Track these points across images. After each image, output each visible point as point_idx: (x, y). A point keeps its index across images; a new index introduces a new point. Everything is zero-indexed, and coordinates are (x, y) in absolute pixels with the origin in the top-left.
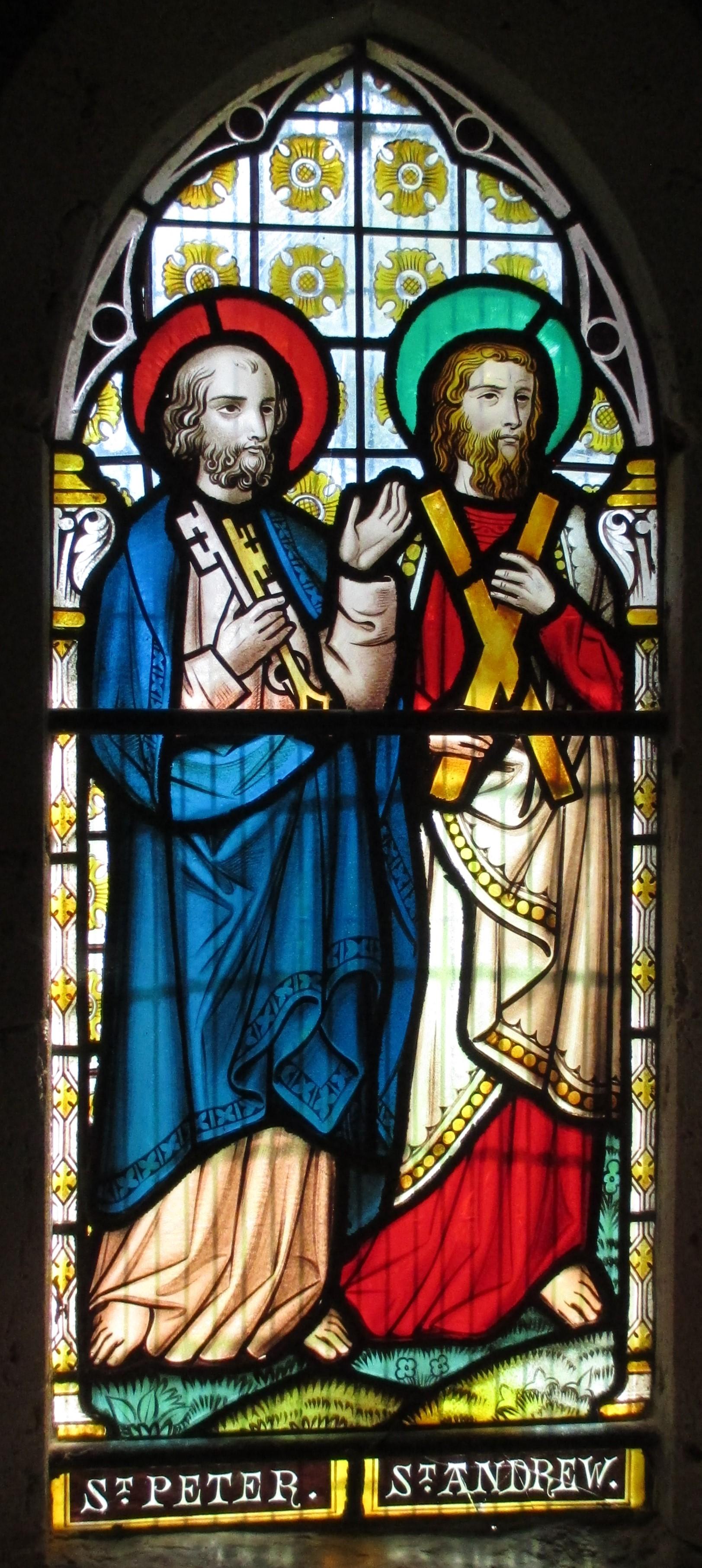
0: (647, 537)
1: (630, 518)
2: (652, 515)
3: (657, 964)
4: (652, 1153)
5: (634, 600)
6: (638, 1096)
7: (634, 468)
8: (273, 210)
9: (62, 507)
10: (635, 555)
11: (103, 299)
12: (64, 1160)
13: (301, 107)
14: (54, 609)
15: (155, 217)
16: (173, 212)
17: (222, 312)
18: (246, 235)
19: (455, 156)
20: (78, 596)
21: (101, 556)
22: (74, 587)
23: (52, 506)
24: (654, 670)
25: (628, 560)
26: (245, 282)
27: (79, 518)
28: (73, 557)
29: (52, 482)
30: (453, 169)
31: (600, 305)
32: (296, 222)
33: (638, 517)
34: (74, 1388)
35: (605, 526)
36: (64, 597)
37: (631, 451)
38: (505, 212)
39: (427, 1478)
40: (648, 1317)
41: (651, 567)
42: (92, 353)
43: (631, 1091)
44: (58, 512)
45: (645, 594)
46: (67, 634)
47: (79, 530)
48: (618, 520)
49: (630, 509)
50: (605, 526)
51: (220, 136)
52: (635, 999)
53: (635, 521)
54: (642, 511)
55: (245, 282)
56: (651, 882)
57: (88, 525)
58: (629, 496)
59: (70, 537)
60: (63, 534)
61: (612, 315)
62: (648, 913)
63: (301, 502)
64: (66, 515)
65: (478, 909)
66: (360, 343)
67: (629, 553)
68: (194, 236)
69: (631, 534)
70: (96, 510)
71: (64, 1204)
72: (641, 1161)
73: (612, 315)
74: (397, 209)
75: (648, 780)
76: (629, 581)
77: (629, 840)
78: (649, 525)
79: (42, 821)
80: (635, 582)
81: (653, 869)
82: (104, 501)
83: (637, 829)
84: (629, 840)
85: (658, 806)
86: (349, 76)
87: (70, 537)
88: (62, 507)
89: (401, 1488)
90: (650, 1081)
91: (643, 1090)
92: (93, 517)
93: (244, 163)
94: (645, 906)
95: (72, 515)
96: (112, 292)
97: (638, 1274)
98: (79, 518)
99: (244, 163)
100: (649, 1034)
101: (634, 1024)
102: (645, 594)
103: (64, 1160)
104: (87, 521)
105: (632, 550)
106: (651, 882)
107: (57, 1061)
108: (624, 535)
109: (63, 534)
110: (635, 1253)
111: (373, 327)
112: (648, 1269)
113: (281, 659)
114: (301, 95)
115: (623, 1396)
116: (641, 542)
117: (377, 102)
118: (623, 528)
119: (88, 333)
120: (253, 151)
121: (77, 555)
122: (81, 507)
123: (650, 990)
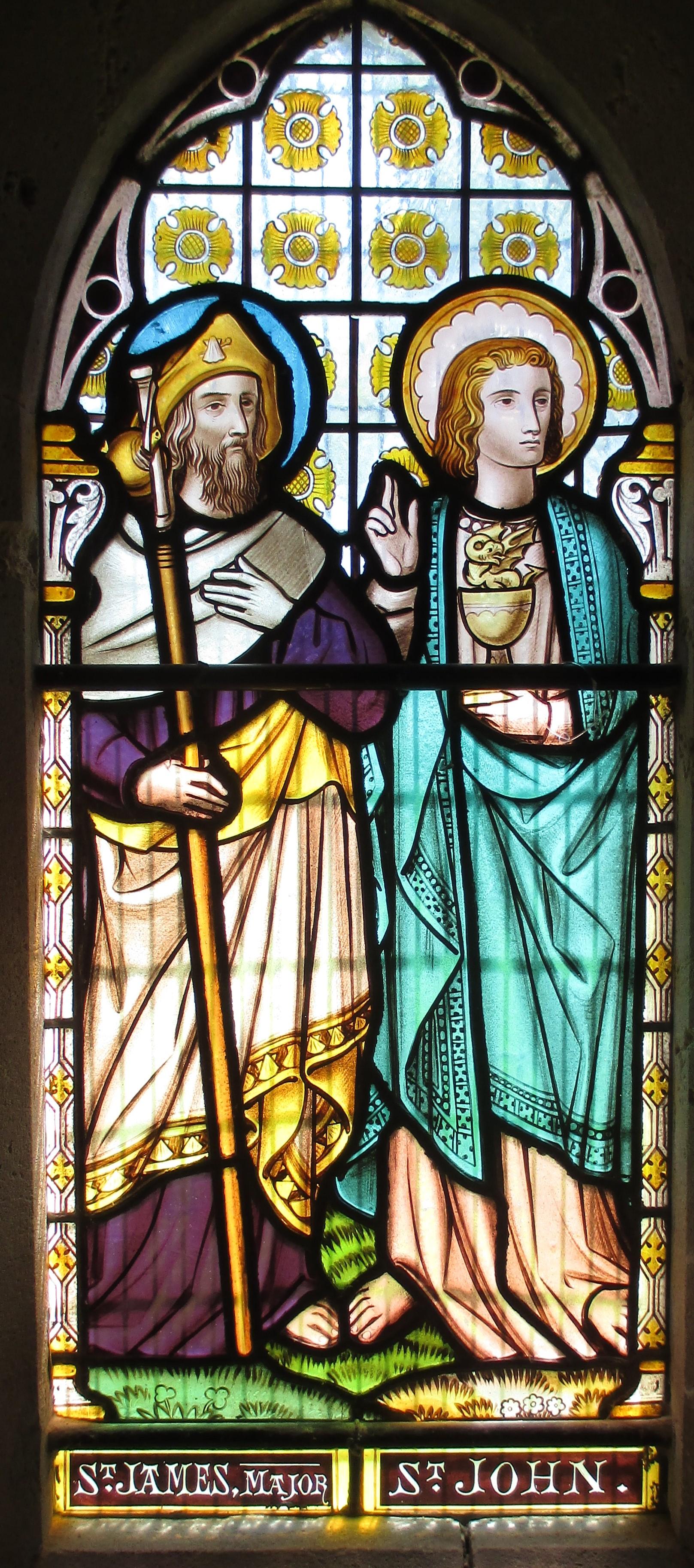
0: (663, 506)
3: (668, 1160)
4: (665, 1152)
5: (649, 575)
7: (651, 433)
9: (52, 478)
10: (649, 525)
11: (93, 272)
12: (55, 762)
15: (151, 184)
16: (171, 176)
20: (70, 573)
21: (92, 527)
22: (66, 563)
23: (41, 476)
25: (644, 532)
27: (70, 489)
28: (67, 528)
29: (40, 453)
30: (456, 125)
33: (654, 485)
34: (71, 1370)
36: (55, 572)
38: (516, 166)
39: (436, 1476)
40: (662, 1060)
41: (666, 558)
42: (83, 324)
44: (48, 484)
45: (659, 570)
46: (57, 608)
47: (72, 504)
48: (634, 487)
50: (619, 487)
52: (648, 989)
53: (651, 491)
56: (668, 781)
57: (80, 498)
58: (644, 465)
59: (61, 512)
60: (54, 507)
63: (306, 478)
64: (60, 487)
68: (191, 218)
69: (645, 502)
70: (89, 483)
71: (55, 808)
72: (652, 1159)
74: (405, 159)
76: (644, 559)
77: (640, 1028)
79: (33, 1273)
83: (649, 1015)
84: (640, 1028)
85: (668, 1178)
87: (61, 512)
88: (52, 478)
89: (408, 1487)
90: (666, 958)
92: (84, 490)
93: (237, 130)
94: (662, 808)
97: (653, 1102)
98: (70, 489)
99: (237, 130)
100: (663, 1213)
102: (659, 570)
103: (55, 762)
106: (668, 781)
107: (50, 846)
109: (54, 507)
113: (284, 1164)
115: (636, 1397)
116: (654, 507)
118: (638, 496)
119: (81, 304)
122: (72, 478)
123: (662, 1187)
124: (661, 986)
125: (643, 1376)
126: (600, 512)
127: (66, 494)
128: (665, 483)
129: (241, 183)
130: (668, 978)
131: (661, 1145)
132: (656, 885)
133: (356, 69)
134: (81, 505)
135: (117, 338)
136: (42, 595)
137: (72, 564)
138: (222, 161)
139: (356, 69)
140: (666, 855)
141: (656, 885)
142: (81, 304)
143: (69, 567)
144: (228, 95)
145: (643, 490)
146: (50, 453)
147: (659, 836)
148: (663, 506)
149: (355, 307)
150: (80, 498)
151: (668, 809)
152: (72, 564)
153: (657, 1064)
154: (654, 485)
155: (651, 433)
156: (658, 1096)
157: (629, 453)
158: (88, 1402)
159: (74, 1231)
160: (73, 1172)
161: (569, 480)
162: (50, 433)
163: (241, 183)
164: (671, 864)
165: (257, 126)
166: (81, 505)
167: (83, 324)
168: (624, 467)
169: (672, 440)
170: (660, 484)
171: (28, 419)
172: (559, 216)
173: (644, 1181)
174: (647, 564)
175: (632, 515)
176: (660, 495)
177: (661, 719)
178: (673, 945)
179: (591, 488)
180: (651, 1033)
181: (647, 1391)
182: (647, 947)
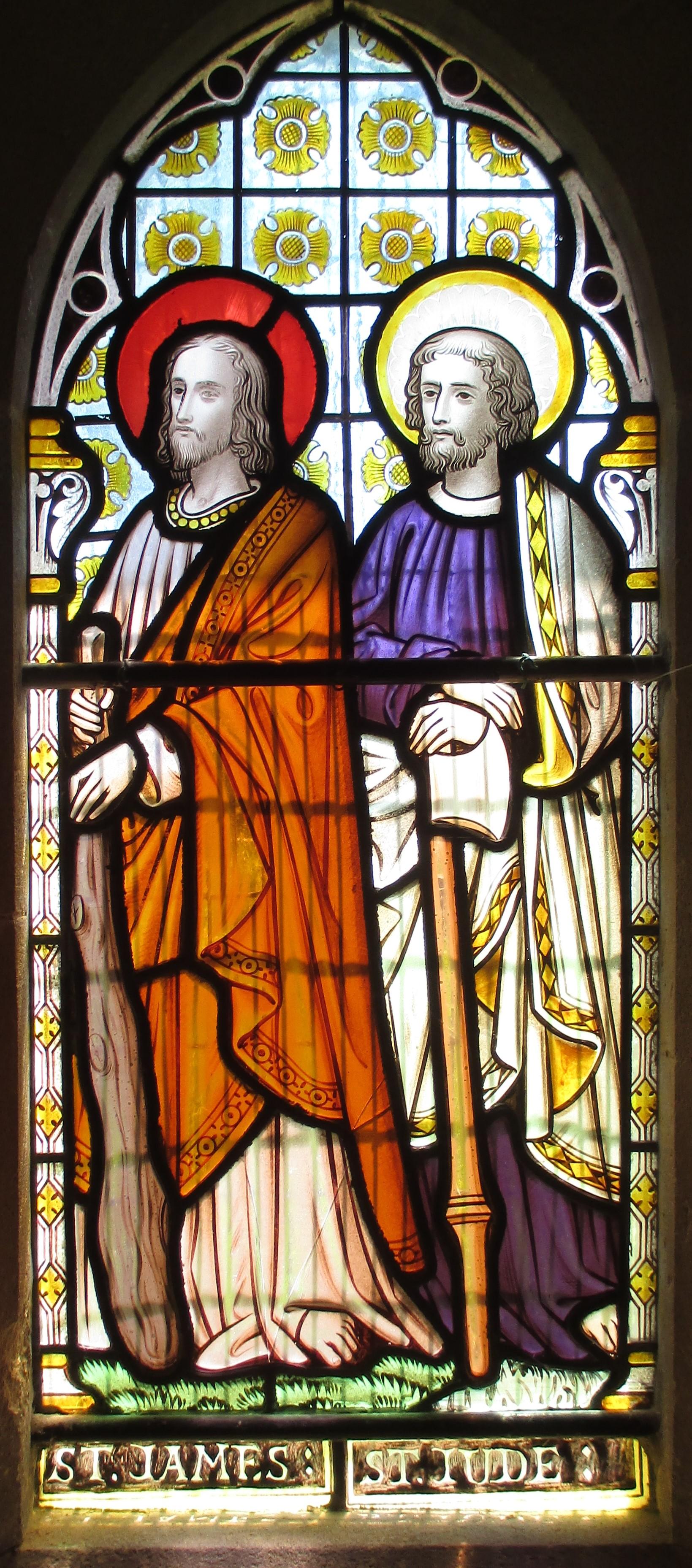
0: (646, 495)
1: (630, 479)
2: (651, 473)
6: (637, 1023)
7: (632, 425)
8: (255, 175)
9: (38, 471)
10: (634, 515)
11: (80, 268)
13: (285, 67)
14: (30, 577)
17: (204, 297)
18: (228, 202)
19: (440, 109)
23: (29, 470)
24: (653, 705)
26: (227, 261)
27: (57, 481)
28: (52, 520)
30: (442, 124)
31: (596, 255)
32: (277, 185)
33: (637, 478)
35: (602, 486)
36: (40, 564)
37: (627, 407)
42: (71, 323)
43: (632, 841)
44: (34, 477)
47: (57, 496)
48: (615, 479)
49: (629, 469)
51: (198, 95)
54: (639, 471)
55: (227, 261)
56: (650, 1190)
57: (65, 489)
60: (40, 501)
61: (608, 263)
62: (649, 865)
64: (43, 480)
65: (479, 1008)
66: (345, 300)
67: (629, 512)
73: (608, 263)
75: (648, 907)
76: (629, 547)
78: (649, 482)
80: (635, 545)
81: (654, 905)
82: (80, 466)
86: (333, 35)
87: (47, 505)
88: (38, 471)
90: (651, 1006)
91: (642, 1105)
92: (69, 483)
93: (227, 126)
95: (47, 481)
96: (90, 259)
98: (57, 481)
99: (227, 126)
101: (634, 1137)
104: (65, 488)
105: (632, 508)
108: (622, 493)
109: (40, 501)
110: (636, 1189)
111: (357, 284)
112: (651, 1294)
114: (286, 50)
116: (638, 497)
117: (362, 58)
118: (621, 485)
119: (67, 302)
120: (237, 114)
121: (56, 518)
122: (57, 472)
123: (652, 859)
124: (647, 861)
125: (632, 1369)
126: (582, 495)
127: (52, 487)
128: (648, 475)
129: (231, 187)
130: (651, 1297)
131: (650, 901)
132: (642, 755)
133: (344, 77)
134: (66, 497)
135: (104, 342)
136: (28, 586)
137: (57, 556)
138: (210, 164)
139: (344, 77)
140: (649, 1078)
141: (642, 755)
142: (67, 302)
143: (54, 559)
144: (214, 97)
145: (626, 483)
146: (35, 447)
147: (642, 1154)
148: (646, 495)
149: (345, 300)
150: (65, 489)
151: (652, 859)
152: (57, 556)
153: (645, 1079)
154: (637, 478)
155: (632, 425)
156: (647, 1207)
157: (610, 445)
158: (193, 558)
159: (62, 1174)
160: (60, 1116)
161: (554, 456)
162: (37, 428)
163: (231, 187)
164: (657, 910)
165: (248, 123)
166: (66, 497)
167: (71, 323)
168: (605, 461)
169: (654, 447)
170: (642, 476)
171: (16, 413)
172: (540, 214)
173: (634, 1024)
174: (631, 552)
175: (617, 506)
176: (642, 485)
177: (644, 1216)
178: (657, 1289)
179: (576, 472)
180: (639, 604)
181: (636, 1381)
182: (634, 815)
